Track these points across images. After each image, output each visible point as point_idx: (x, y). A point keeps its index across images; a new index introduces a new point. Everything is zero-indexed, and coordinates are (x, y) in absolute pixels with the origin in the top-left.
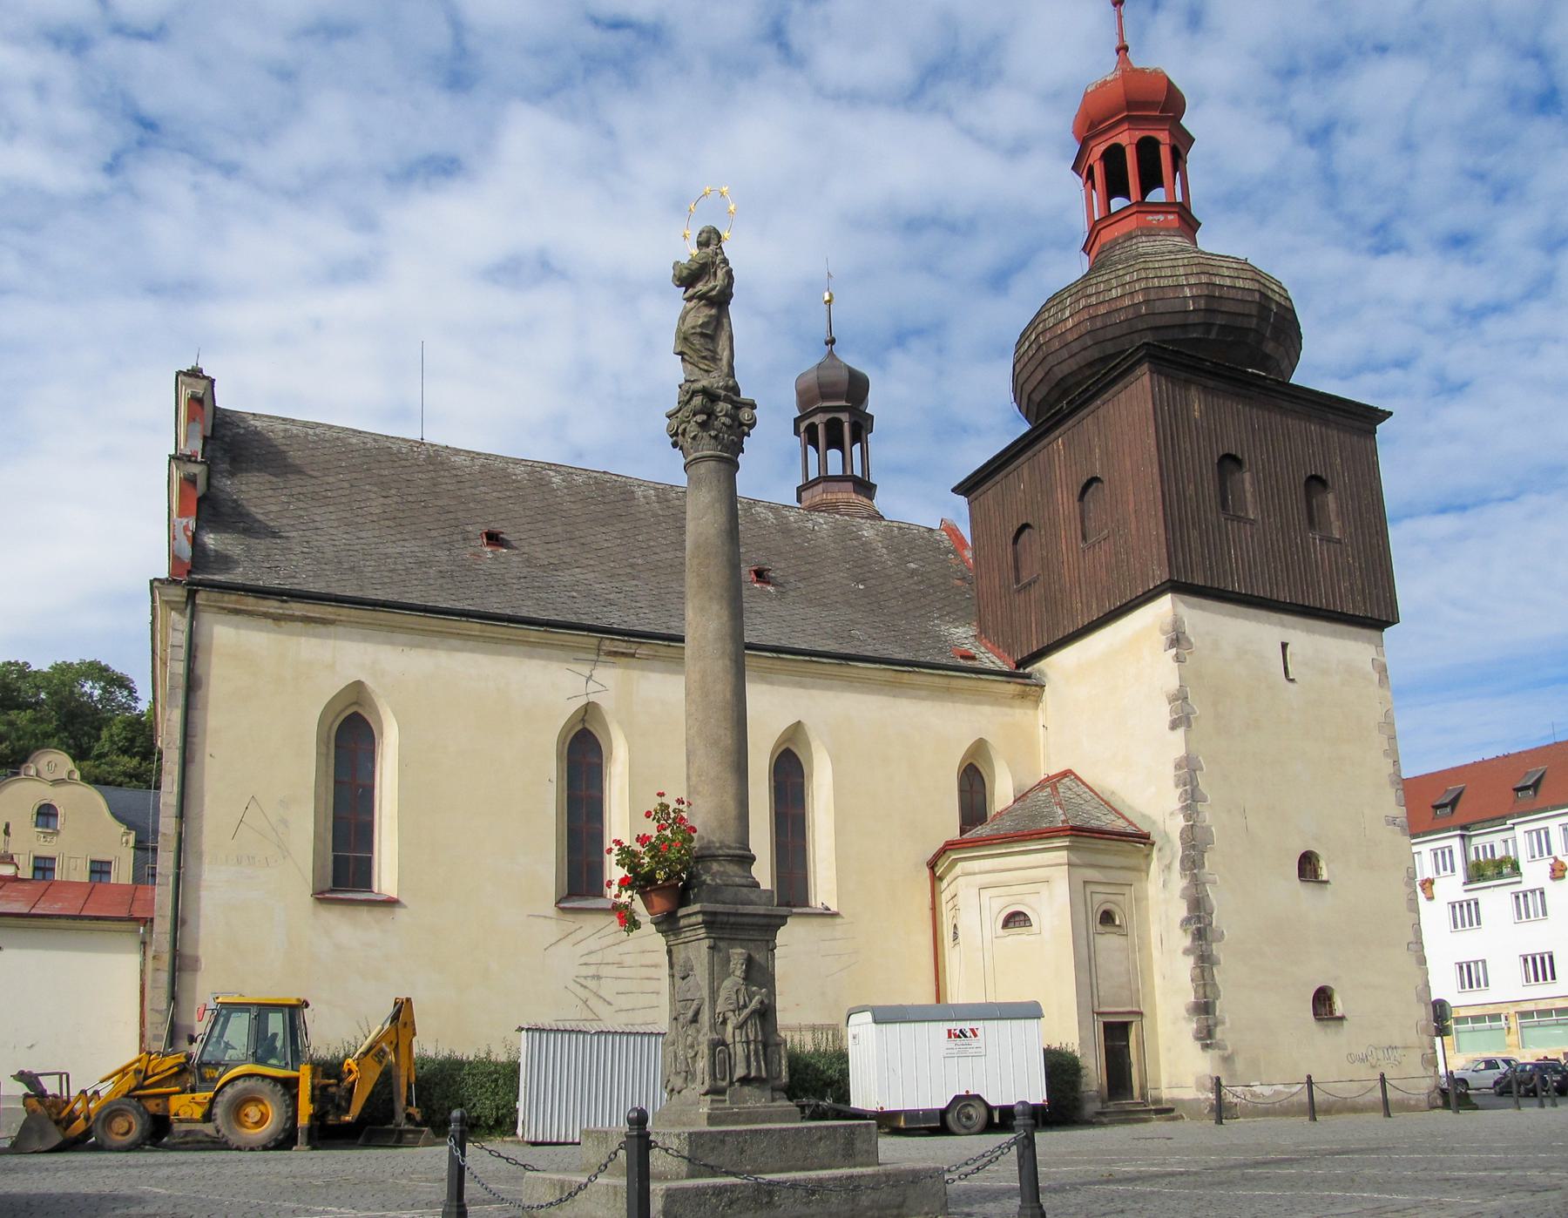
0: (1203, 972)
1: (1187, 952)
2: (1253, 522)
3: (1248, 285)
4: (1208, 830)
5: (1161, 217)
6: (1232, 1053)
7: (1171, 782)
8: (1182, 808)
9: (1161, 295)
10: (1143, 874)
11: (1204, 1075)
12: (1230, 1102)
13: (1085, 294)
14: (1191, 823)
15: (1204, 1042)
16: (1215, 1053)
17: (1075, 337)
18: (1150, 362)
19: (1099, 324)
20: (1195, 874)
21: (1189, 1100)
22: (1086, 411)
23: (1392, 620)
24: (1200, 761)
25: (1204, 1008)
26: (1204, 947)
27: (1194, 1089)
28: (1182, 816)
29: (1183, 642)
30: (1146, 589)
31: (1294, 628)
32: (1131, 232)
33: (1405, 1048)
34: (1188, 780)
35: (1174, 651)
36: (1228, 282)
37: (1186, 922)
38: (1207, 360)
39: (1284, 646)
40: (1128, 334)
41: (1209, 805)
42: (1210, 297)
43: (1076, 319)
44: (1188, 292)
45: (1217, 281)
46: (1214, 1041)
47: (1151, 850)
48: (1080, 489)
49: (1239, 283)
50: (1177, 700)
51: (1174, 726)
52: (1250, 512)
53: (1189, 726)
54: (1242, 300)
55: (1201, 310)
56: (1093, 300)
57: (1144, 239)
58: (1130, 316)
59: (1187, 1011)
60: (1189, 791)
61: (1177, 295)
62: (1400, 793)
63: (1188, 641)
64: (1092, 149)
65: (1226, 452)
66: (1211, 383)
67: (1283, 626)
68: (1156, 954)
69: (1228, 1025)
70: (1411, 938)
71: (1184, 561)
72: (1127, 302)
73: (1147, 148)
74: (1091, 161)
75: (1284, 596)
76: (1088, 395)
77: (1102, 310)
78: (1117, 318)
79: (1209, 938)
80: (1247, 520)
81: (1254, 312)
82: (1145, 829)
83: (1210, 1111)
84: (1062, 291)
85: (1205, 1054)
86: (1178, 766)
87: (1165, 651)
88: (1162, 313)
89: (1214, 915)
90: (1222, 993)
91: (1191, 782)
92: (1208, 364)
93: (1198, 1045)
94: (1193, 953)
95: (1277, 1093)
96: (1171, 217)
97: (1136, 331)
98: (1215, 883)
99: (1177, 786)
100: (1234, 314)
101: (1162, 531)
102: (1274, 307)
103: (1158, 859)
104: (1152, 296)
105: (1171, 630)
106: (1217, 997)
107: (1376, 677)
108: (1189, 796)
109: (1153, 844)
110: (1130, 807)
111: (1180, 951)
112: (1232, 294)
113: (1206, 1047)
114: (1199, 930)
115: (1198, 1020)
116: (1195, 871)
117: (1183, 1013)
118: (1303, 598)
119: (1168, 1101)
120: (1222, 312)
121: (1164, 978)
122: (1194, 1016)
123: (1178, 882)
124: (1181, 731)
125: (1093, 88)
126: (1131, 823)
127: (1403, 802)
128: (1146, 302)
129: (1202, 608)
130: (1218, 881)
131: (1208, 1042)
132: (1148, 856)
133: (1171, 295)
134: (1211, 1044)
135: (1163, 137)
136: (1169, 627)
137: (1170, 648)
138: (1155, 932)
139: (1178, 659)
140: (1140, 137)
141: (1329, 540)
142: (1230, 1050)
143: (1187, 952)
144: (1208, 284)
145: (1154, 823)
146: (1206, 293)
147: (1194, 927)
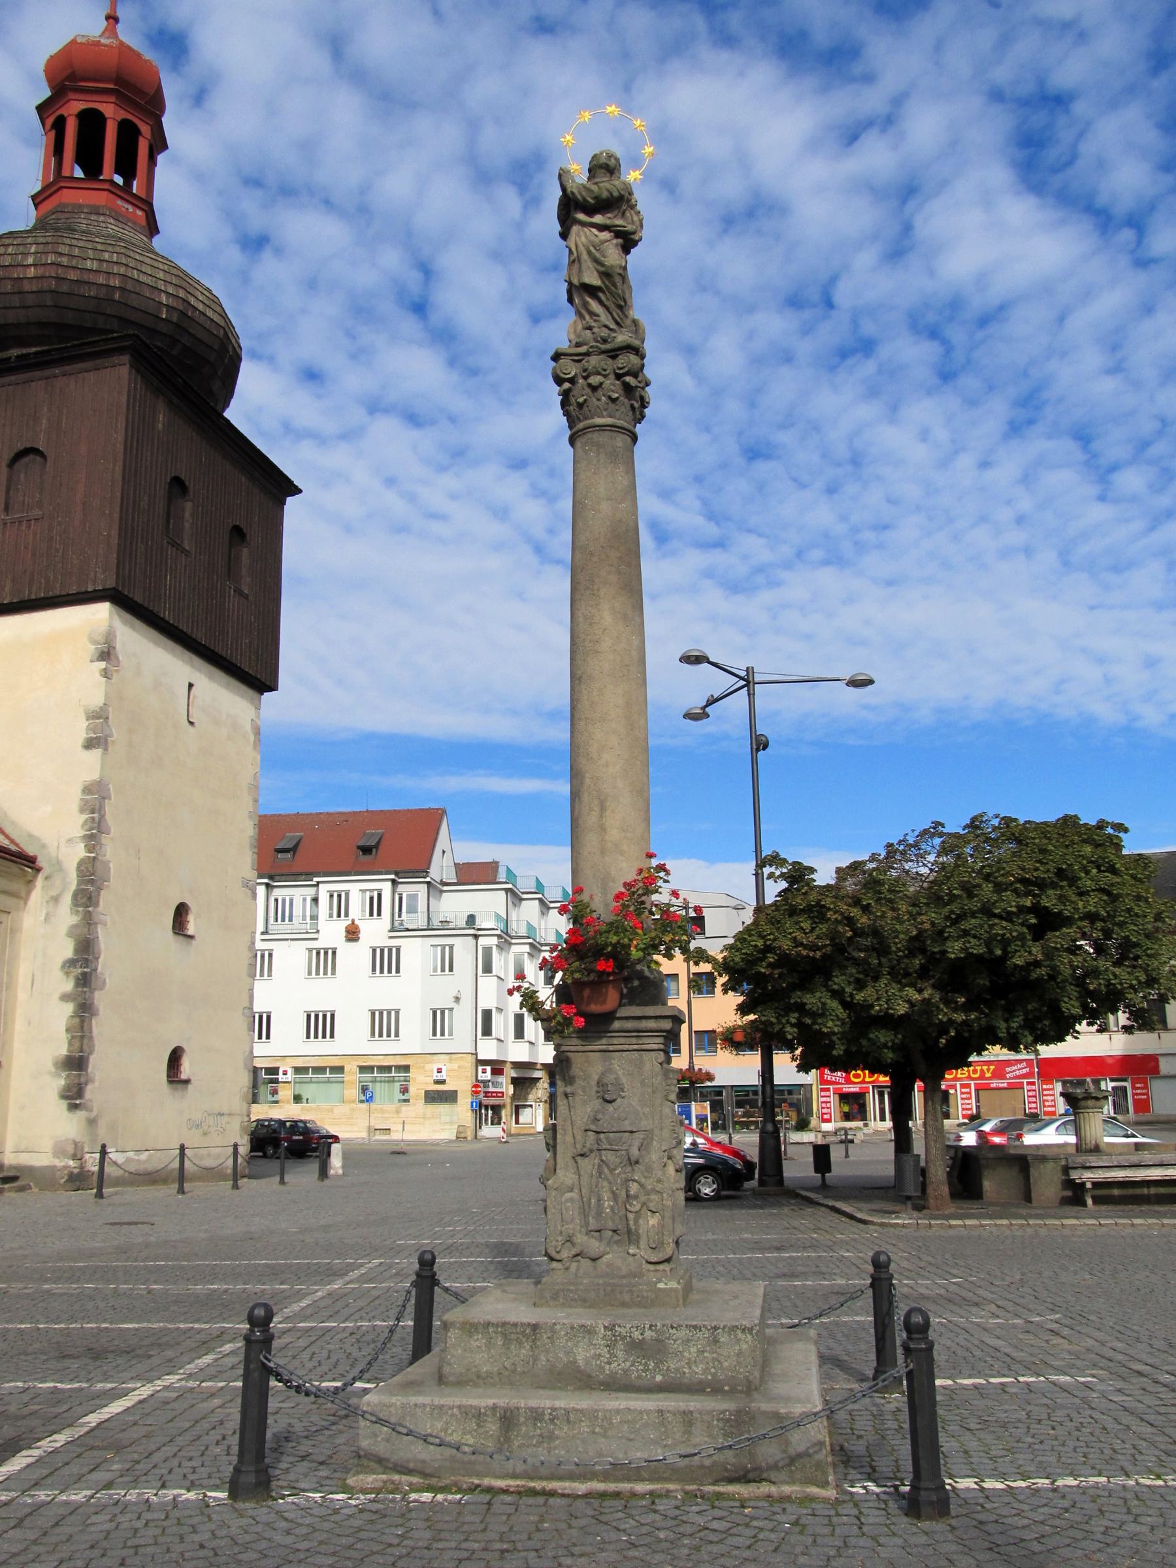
0: (82, 1022)
1: (65, 998)
2: (187, 553)
3: (216, 318)
4: (106, 864)
5: (131, 209)
6: (97, 1116)
7: (75, 806)
8: (85, 837)
9: (137, 290)
10: (22, 902)
11: (67, 1140)
12: (89, 1171)
13: (56, 250)
14: (93, 855)
15: (73, 1101)
16: (81, 1115)
17: (34, 289)
18: (132, 355)
19: (65, 288)
20: (89, 911)
21: (41, 1167)
22: (38, 374)
23: (273, 687)
24: (109, 790)
25: (76, 1063)
26: (88, 994)
27: (50, 1155)
28: (82, 845)
29: (112, 657)
30: (83, 590)
31: (200, 671)
32: (98, 207)
33: (230, 1115)
34: (97, 807)
35: (103, 665)
36: (201, 307)
37: (70, 964)
38: (180, 377)
39: (191, 686)
40: (92, 312)
41: (112, 839)
42: (183, 314)
43: (40, 271)
44: (164, 299)
45: (192, 301)
46: (82, 1101)
47: (35, 877)
48: (12, 454)
49: (210, 313)
50: (98, 718)
51: (89, 745)
52: (186, 542)
53: (106, 749)
54: (209, 331)
55: (172, 322)
56: (64, 260)
57: (112, 221)
58: (101, 296)
59: (56, 1064)
60: (97, 820)
61: (153, 297)
62: (255, 856)
63: (117, 658)
64: (68, 101)
65: (177, 474)
66: (175, 400)
67: (193, 666)
68: (22, 995)
69: (97, 1084)
70: (247, 1005)
71: (130, 571)
72: (101, 280)
73: (128, 132)
74: (63, 111)
75: (201, 636)
76: (46, 359)
77: (73, 275)
78: (85, 290)
79: (93, 986)
80: (184, 550)
81: (216, 347)
82: (30, 851)
83: (67, 1181)
84: (163, 257)
85: (70, 1115)
86: (87, 790)
87: (92, 661)
88: (135, 308)
89: (100, 960)
90: (96, 1048)
91: (100, 810)
92: (180, 380)
93: (64, 1104)
94: (74, 1000)
95: (128, 1160)
96: (139, 213)
97: (104, 314)
98: (106, 925)
99: (82, 811)
100: (200, 340)
101: (115, 533)
102: (230, 349)
103: (43, 888)
104: (129, 287)
105: (103, 641)
106: (91, 1053)
107: (252, 738)
108: (96, 825)
109: (38, 870)
110: (13, 823)
111: (57, 995)
112: (202, 320)
113: (73, 1107)
114: (84, 974)
115: (68, 1076)
116: (90, 909)
117: (50, 1066)
118: (222, 649)
119: (11, 1167)
120: (189, 333)
121: (29, 1023)
122: (65, 1071)
123: (67, 917)
124: (97, 753)
125: (84, 40)
126: (12, 841)
127: (255, 867)
128: (122, 289)
129: (133, 627)
130: (109, 924)
131: (78, 1102)
132: (30, 883)
133: (148, 295)
134: (80, 1104)
135: (145, 129)
136: (100, 638)
137: (98, 660)
138: (24, 971)
139: (106, 674)
140: (123, 117)
141: (239, 592)
142: (94, 1113)
143: (65, 998)
144: (184, 300)
145: (44, 846)
146: (181, 308)
147: (80, 970)
